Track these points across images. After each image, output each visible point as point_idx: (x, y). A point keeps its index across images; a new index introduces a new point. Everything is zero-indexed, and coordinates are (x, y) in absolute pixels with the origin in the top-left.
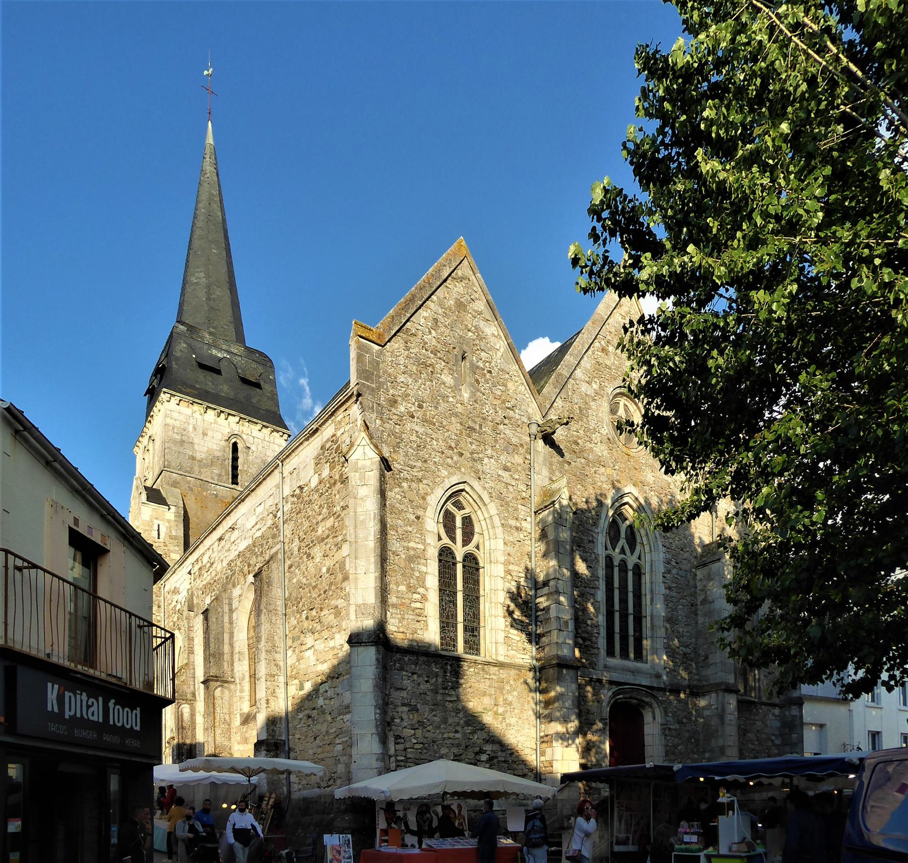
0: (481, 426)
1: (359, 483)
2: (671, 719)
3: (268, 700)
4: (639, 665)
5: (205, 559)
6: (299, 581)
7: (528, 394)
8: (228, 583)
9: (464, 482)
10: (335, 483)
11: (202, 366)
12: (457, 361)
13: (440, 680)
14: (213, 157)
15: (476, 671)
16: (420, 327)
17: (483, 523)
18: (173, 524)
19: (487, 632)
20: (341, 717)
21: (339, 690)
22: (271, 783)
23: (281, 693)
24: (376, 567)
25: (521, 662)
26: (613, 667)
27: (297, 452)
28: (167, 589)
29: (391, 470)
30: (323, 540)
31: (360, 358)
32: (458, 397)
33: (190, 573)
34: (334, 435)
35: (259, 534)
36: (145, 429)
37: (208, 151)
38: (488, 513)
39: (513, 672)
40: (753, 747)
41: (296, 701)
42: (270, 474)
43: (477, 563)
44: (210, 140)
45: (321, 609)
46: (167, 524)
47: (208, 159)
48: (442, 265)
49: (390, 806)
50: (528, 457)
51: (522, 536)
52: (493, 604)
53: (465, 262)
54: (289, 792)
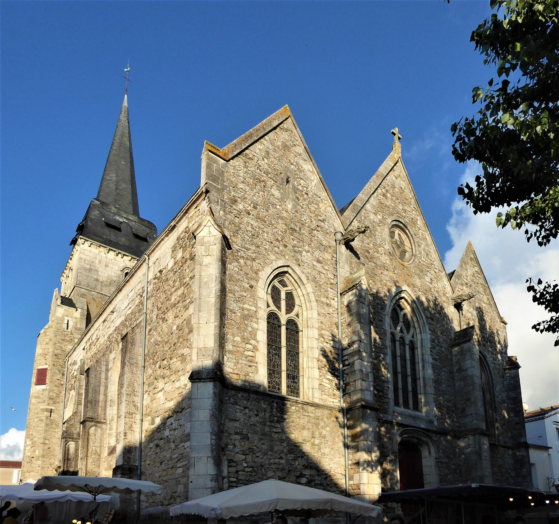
0: (300, 229)
1: (204, 253)
2: (442, 455)
3: (125, 433)
4: (417, 413)
5: (94, 337)
6: (156, 340)
7: (334, 213)
8: (108, 349)
9: (288, 266)
10: (186, 261)
11: (108, 225)
12: (283, 182)
13: (268, 415)
14: (127, 113)
15: (297, 409)
16: (256, 155)
17: (302, 298)
19: (305, 380)
20: (182, 444)
21: (182, 422)
22: (123, 501)
23: (137, 428)
24: (216, 318)
25: (332, 405)
26: (399, 414)
27: (159, 247)
28: (69, 363)
29: (231, 249)
30: (175, 305)
31: (209, 166)
32: (284, 207)
33: (84, 349)
34: (187, 227)
35: (130, 311)
36: (68, 264)
37: (123, 110)
39: (326, 412)
41: (148, 434)
42: (140, 267)
43: (297, 327)
44: (125, 104)
45: (171, 359)
46: (74, 320)
47: (123, 114)
48: (274, 119)
50: (335, 256)
51: (331, 310)
52: (310, 359)
53: (289, 119)
54: (139, 509)
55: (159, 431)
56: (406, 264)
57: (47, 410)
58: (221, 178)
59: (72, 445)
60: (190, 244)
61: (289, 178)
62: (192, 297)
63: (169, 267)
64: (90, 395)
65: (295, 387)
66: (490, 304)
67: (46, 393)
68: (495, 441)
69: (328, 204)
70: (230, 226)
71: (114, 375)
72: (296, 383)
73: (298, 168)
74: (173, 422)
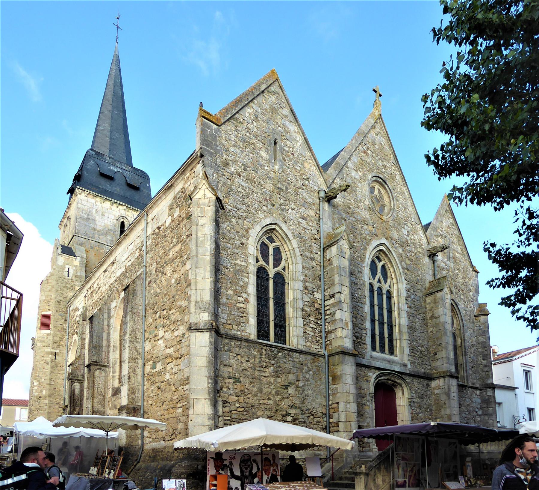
0: (286, 188)
4: (391, 357)
5: (95, 286)
8: (109, 299)
9: (276, 224)
10: (183, 220)
11: (102, 175)
13: (257, 360)
16: (245, 119)
18: (78, 268)
19: (291, 328)
21: (181, 367)
24: (211, 274)
26: (377, 358)
28: (71, 309)
29: (224, 209)
30: (173, 260)
32: (272, 167)
33: (85, 297)
34: (183, 188)
35: (130, 263)
38: (292, 246)
39: (309, 357)
40: (465, 416)
43: (284, 280)
45: (170, 310)
46: (74, 268)
49: (218, 456)
50: (318, 212)
54: (143, 444)
55: (160, 374)
56: (384, 218)
57: (51, 353)
58: (214, 143)
59: (77, 386)
60: (186, 204)
61: (276, 139)
62: (189, 254)
63: (167, 225)
64: (94, 340)
65: (281, 335)
66: (463, 254)
67: (50, 338)
68: (464, 383)
69: (312, 163)
70: (223, 188)
71: (116, 323)
72: (283, 331)
73: (285, 130)
74: (173, 366)
